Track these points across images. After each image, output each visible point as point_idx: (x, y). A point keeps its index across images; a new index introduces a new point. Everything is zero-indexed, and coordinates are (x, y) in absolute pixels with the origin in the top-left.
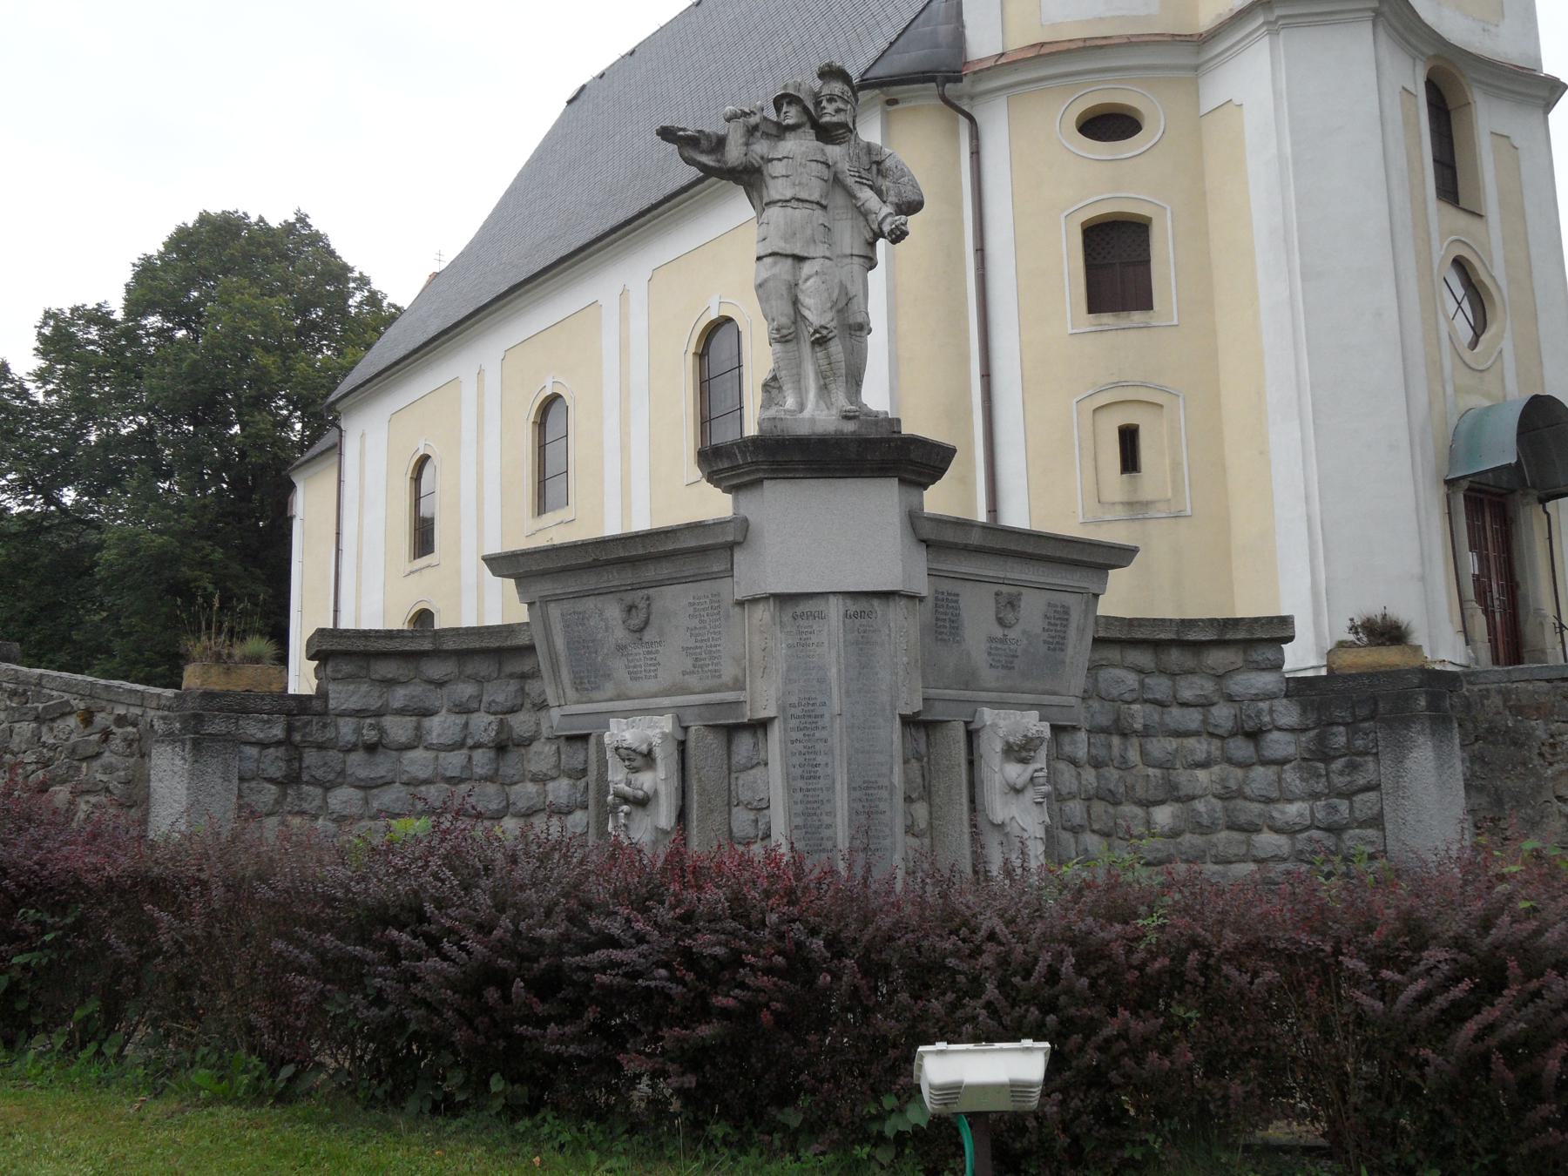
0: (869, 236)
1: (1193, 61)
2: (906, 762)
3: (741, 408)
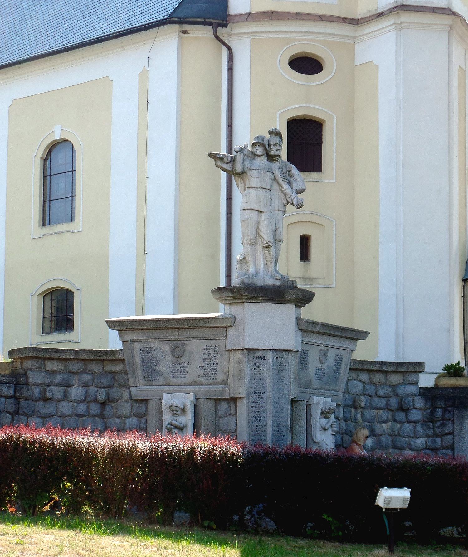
0: (285, 202)
1: (352, 34)
3: (73, 196)
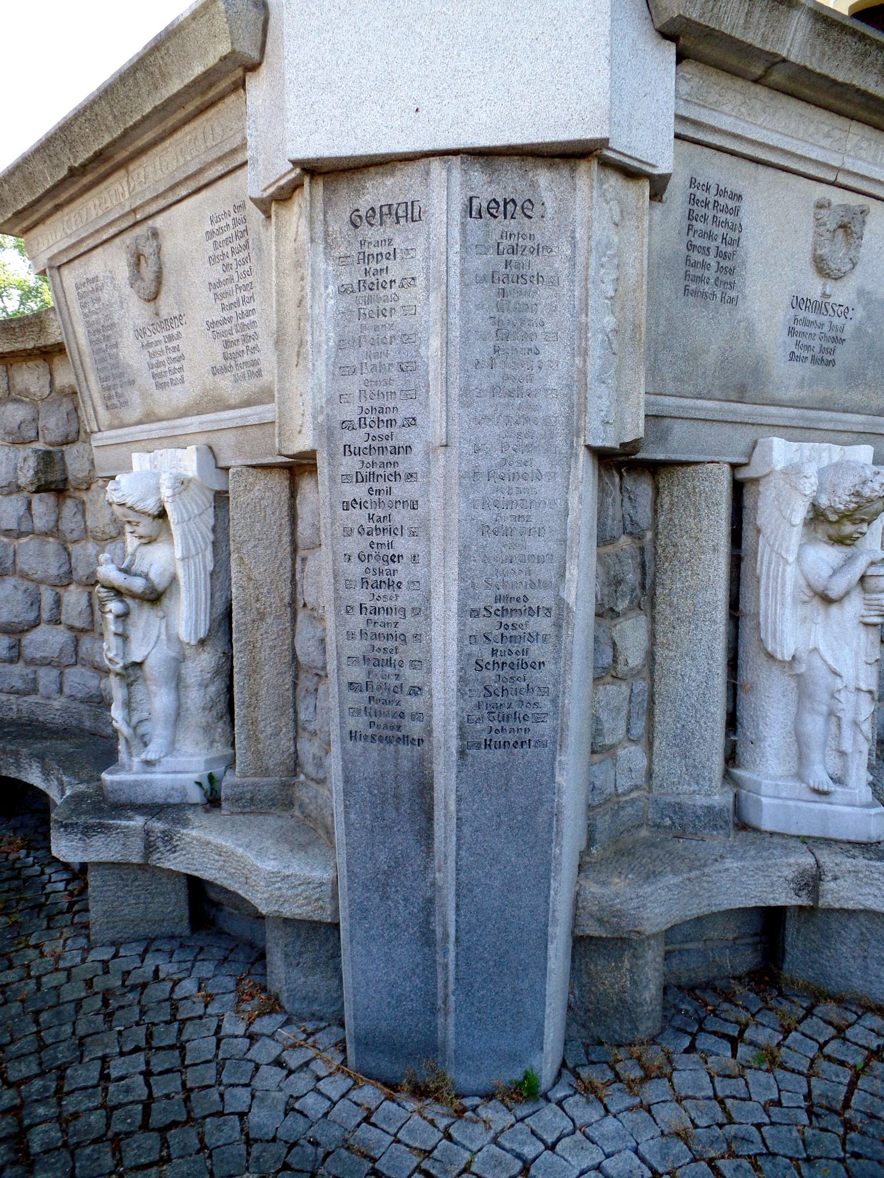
2: (604, 540)
